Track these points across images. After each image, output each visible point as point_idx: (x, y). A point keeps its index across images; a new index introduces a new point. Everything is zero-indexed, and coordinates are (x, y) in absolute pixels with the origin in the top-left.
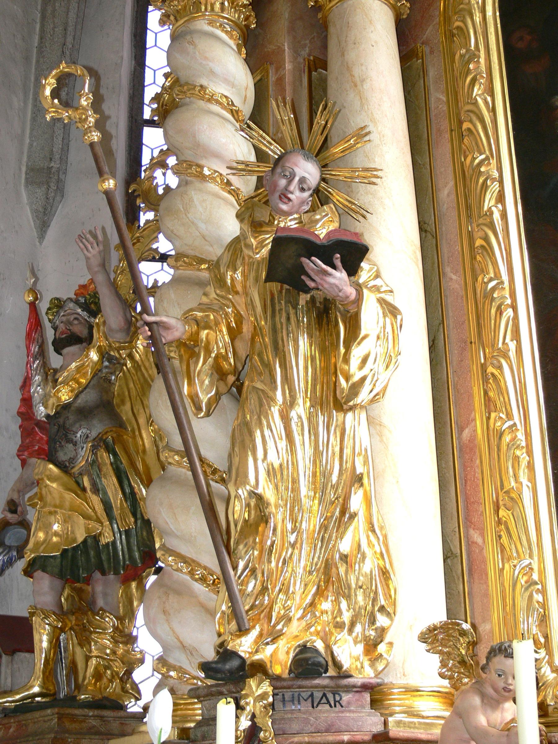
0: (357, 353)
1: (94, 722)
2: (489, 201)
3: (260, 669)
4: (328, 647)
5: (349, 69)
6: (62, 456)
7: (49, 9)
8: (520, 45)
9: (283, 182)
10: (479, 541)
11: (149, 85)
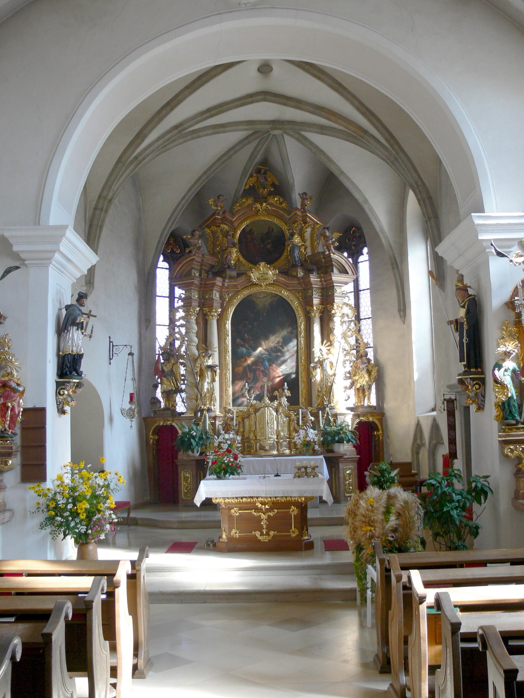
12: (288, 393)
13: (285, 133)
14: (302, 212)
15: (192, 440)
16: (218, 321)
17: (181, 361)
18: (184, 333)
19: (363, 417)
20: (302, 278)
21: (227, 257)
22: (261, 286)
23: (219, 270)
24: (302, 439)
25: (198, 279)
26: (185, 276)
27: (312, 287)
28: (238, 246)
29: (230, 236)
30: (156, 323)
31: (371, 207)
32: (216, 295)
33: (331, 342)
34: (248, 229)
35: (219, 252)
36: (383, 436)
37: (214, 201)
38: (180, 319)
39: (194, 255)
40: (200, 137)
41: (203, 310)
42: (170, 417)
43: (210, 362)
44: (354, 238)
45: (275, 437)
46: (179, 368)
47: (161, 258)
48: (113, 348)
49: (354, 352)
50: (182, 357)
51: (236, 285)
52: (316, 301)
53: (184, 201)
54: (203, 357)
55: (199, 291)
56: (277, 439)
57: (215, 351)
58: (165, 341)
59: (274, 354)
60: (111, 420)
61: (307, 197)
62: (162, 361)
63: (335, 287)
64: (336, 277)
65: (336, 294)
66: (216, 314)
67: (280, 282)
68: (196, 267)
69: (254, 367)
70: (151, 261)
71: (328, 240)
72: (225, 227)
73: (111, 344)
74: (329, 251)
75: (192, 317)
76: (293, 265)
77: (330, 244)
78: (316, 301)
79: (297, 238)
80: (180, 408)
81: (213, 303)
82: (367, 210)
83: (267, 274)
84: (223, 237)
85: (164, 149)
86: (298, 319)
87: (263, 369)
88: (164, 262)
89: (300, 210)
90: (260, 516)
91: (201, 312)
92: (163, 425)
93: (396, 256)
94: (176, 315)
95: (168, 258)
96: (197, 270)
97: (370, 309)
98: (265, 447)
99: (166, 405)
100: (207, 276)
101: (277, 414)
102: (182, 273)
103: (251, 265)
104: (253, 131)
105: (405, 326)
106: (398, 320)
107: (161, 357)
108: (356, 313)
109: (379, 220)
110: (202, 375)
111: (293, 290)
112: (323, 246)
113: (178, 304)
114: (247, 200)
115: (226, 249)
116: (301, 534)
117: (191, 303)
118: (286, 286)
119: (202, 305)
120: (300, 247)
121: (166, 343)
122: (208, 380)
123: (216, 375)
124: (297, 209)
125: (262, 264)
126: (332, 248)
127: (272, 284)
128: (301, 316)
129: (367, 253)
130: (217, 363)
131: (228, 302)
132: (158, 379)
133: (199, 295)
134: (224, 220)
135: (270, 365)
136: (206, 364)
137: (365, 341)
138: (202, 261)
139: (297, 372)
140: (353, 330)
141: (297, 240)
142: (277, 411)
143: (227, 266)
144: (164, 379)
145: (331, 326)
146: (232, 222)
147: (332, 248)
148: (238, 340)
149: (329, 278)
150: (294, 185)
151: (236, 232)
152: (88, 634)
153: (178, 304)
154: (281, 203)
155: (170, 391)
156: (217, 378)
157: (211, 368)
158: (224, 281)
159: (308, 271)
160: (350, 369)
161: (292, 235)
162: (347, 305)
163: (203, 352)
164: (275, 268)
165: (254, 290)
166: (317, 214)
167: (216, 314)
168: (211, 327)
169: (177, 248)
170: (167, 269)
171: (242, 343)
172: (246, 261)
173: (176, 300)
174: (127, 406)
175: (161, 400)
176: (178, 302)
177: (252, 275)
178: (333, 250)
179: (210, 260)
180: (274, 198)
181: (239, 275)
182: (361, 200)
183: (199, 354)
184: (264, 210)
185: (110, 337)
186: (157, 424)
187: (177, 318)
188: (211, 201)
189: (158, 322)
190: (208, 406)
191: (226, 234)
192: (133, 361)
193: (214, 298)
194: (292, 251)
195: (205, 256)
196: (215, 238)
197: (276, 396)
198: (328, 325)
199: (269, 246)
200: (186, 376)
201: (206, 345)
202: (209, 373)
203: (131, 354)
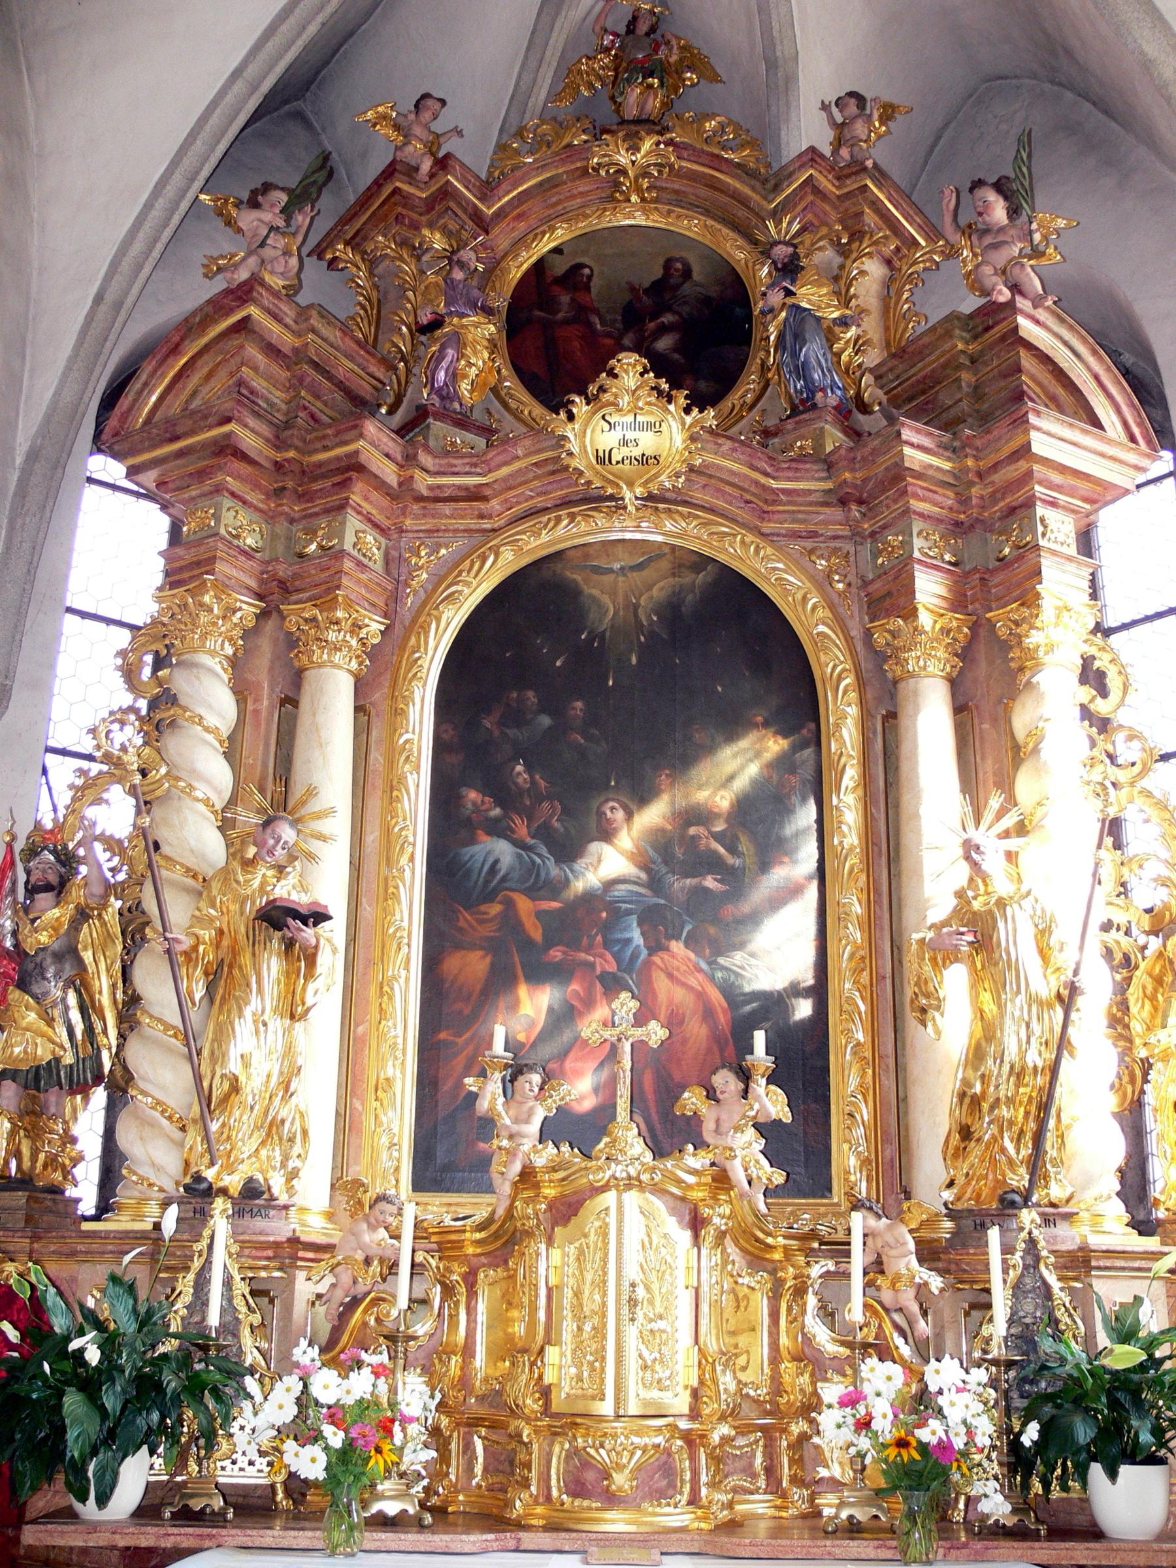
0: (311, 987)
1: (49, 1203)
2: (404, 861)
3: (224, 1191)
4: (266, 1180)
5: (317, 729)
6: (36, 989)
7: (20, 521)
8: (445, 736)
9: (271, 842)
10: (360, 1108)
11: (109, 621)
15: (72, 1401)
16: (361, 686)
24: (883, 1425)
27: (907, 512)
34: (560, 266)
45: (682, 1403)
51: (474, 495)
56: (694, 1414)
59: (680, 885)
63: (1041, 510)
87: (612, 967)
118: (758, 509)
119: (274, 593)
135: (656, 947)
139: (819, 991)
148: (473, 795)
171: (497, 812)
197: (695, 1120)
198: (1003, 720)
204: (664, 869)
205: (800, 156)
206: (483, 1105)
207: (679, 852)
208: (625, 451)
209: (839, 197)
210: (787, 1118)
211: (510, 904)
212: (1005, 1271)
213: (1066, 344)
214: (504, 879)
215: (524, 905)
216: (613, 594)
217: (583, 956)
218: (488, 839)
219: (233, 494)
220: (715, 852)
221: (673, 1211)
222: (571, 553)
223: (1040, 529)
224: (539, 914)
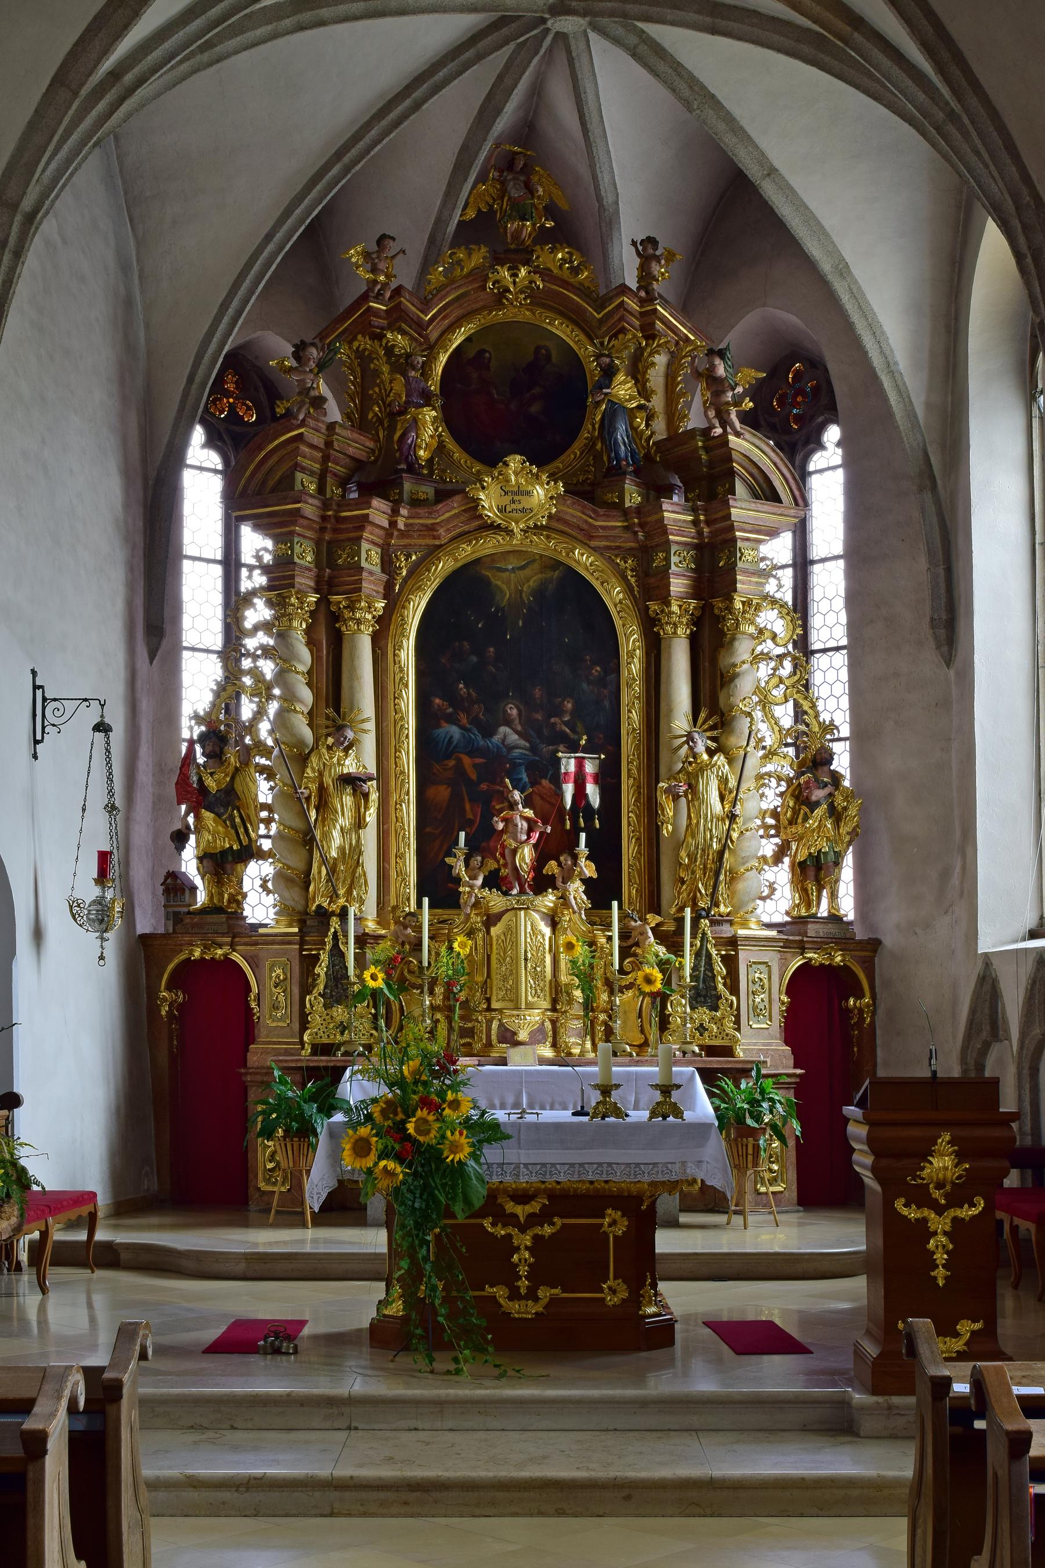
12: (589, 870)
13: (595, 28)
14: (642, 302)
17: (263, 761)
18: (269, 676)
19: (815, 950)
20: (639, 510)
21: (404, 436)
22: (510, 532)
23: (382, 474)
25: (316, 502)
26: (273, 491)
28: (439, 403)
29: (414, 368)
30: (181, 641)
31: (859, 288)
32: (370, 557)
33: (722, 715)
34: (471, 353)
35: (380, 421)
36: (874, 1013)
37: (367, 255)
38: (256, 628)
39: (303, 423)
40: (322, 23)
41: (329, 603)
42: (223, 935)
43: (350, 766)
44: (797, 399)
46: (255, 781)
47: (198, 434)
48: (44, 708)
49: (791, 751)
50: (260, 748)
51: (431, 528)
52: (678, 585)
53: (270, 247)
54: (329, 748)
55: (318, 543)
57: (365, 731)
58: (209, 697)
60: (38, 934)
61: (658, 253)
62: (201, 760)
63: (739, 544)
64: (743, 509)
65: (740, 564)
66: (369, 617)
67: (566, 522)
68: (306, 463)
69: (484, 786)
70: (165, 440)
71: (724, 392)
72: (399, 340)
73: (39, 693)
74: (724, 423)
75: (295, 624)
76: (609, 469)
77: (728, 403)
78: (678, 585)
79: (624, 383)
80: (260, 908)
81: (360, 581)
82: (845, 298)
83: (528, 493)
84: (391, 372)
85: (205, 57)
86: (622, 639)
88: (206, 451)
89: (635, 295)
90: (509, 1236)
91: (323, 608)
92: (202, 960)
93: (929, 449)
94: (244, 618)
95: (221, 438)
96: (312, 473)
97: (843, 618)
98: (515, 1034)
99: (211, 896)
100: (343, 496)
101: (554, 931)
102: (264, 483)
103: (477, 467)
104: (494, 16)
105: (952, 673)
106: (930, 656)
107: (198, 749)
108: (799, 631)
109: (883, 333)
110: (323, 804)
111: (608, 548)
112: (706, 409)
113: (252, 580)
114: (470, 255)
115: (403, 412)
116: (636, 1300)
117: (293, 577)
118: (586, 537)
119: (325, 586)
120: (631, 414)
121: (214, 705)
122: (344, 820)
123: (366, 808)
124: (624, 289)
125: (515, 461)
126: (733, 416)
127: (543, 528)
128: (631, 634)
129: (839, 444)
130: (372, 769)
131: (405, 580)
132: (187, 814)
133: (317, 554)
134: (397, 317)
136: (339, 770)
137: (825, 717)
138: (329, 444)
140: (788, 682)
141: (623, 389)
142: (554, 924)
143: (403, 466)
144: (207, 815)
145: (724, 662)
146: (421, 327)
147: (733, 416)
148: (437, 701)
149: (720, 514)
150: (617, 211)
151: (432, 358)
152: (31, 1522)
153: (252, 580)
154: (575, 271)
155: (224, 853)
156: (371, 816)
157: (351, 781)
158: (395, 512)
159: (657, 492)
160: (778, 802)
161: (609, 373)
162: (774, 602)
163: (328, 735)
164: (553, 477)
165: (488, 545)
166: (685, 309)
167: (369, 617)
168: (353, 658)
169: (249, 408)
170: (215, 471)
171: (450, 710)
172: (465, 455)
173: (244, 572)
174: (89, 892)
175: (198, 881)
176: (250, 577)
177: (482, 496)
178: (737, 424)
179: (355, 444)
180: (553, 251)
181: (442, 496)
182: (826, 266)
183: (317, 740)
184: (522, 292)
185: (34, 673)
186: (182, 957)
187: (248, 624)
188: (354, 254)
189: (189, 638)
190: (342, 901)
191: (402, 364)
192: (108, 751)
193: (364, 564)
194: (607, 426)
195: (338, 430)
196: (367, 376)
199: (535, 408)
200: (276, 807)
201: (337, 710)
202: (348, 800)
203: (102, 727)
204: (538, 741)
205: (616, 288)
206: (455, 872)
207: (546, 732)
208: (513, 506)
209: (641, 313)
210: (595, 876)
211: (459, 760)
212: (692, 946)
213: (757, 447)
214: (456, 746)
215: (467, 761)
216: (508, 583)
217: (497, 787)
218: (445, 725)
219: (299, 535)
220: (565, 732)
221: (542, 919)
222: (485, 559)
223: (739, 555)
224: (475, 766)
